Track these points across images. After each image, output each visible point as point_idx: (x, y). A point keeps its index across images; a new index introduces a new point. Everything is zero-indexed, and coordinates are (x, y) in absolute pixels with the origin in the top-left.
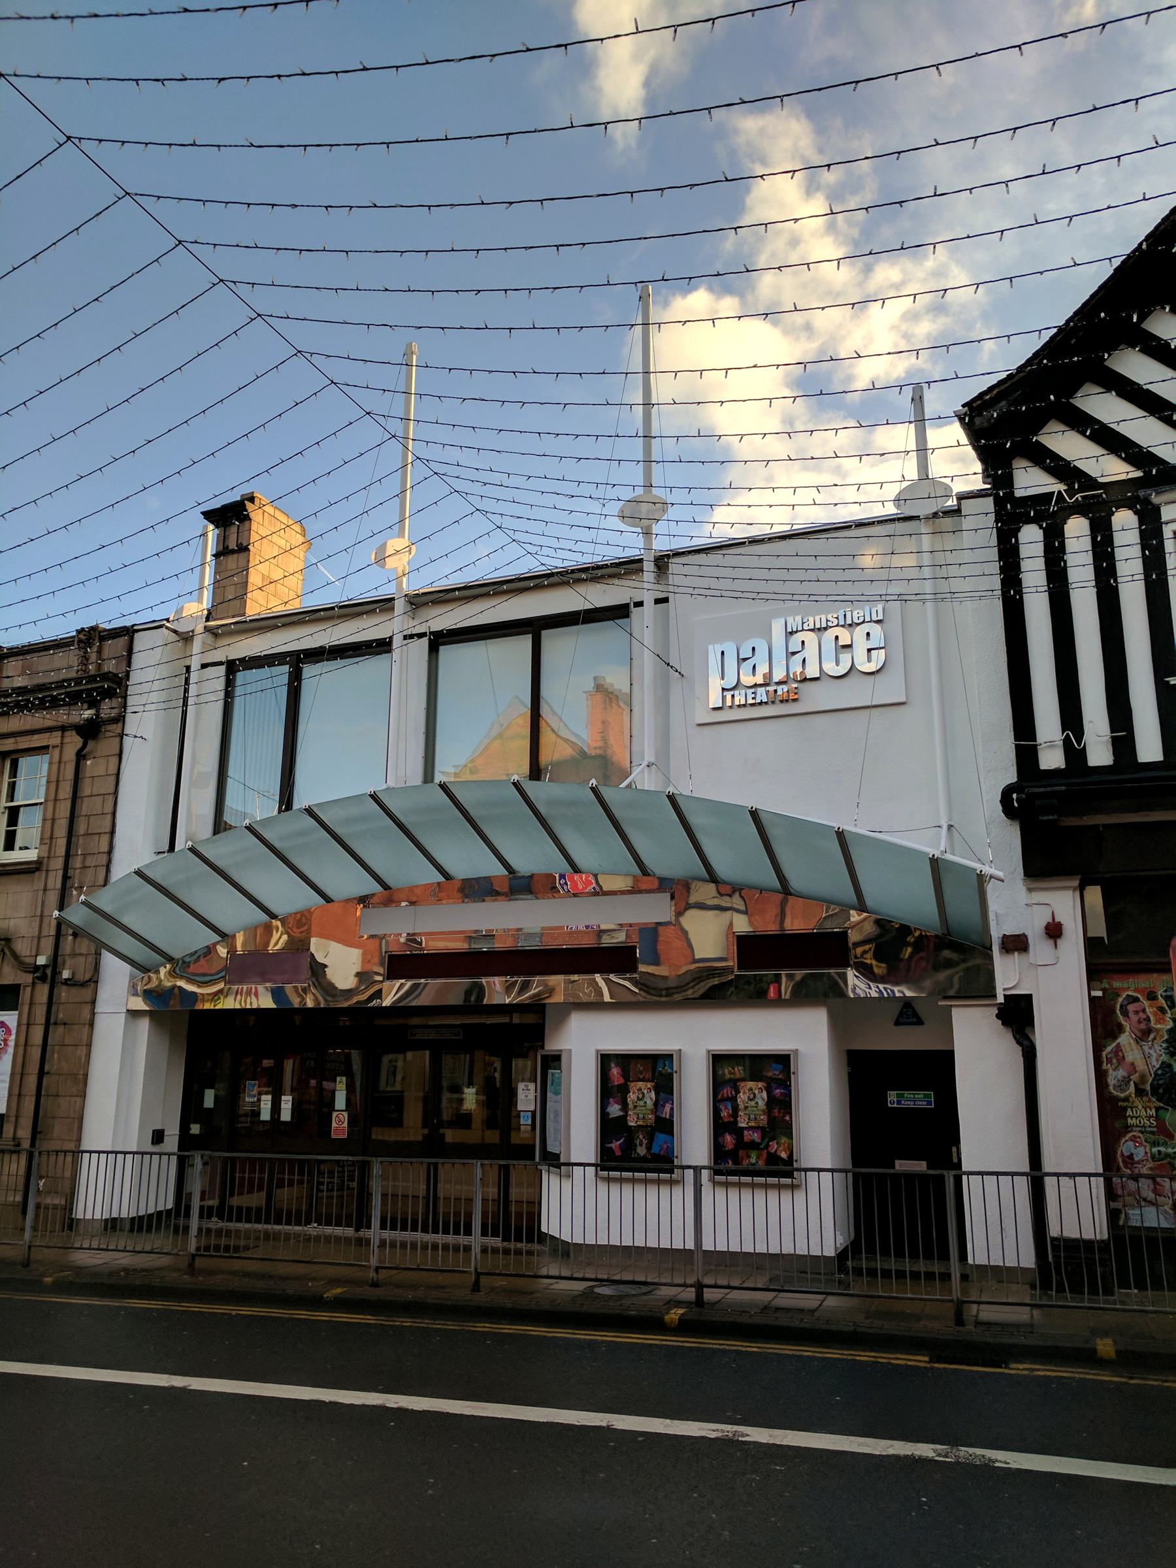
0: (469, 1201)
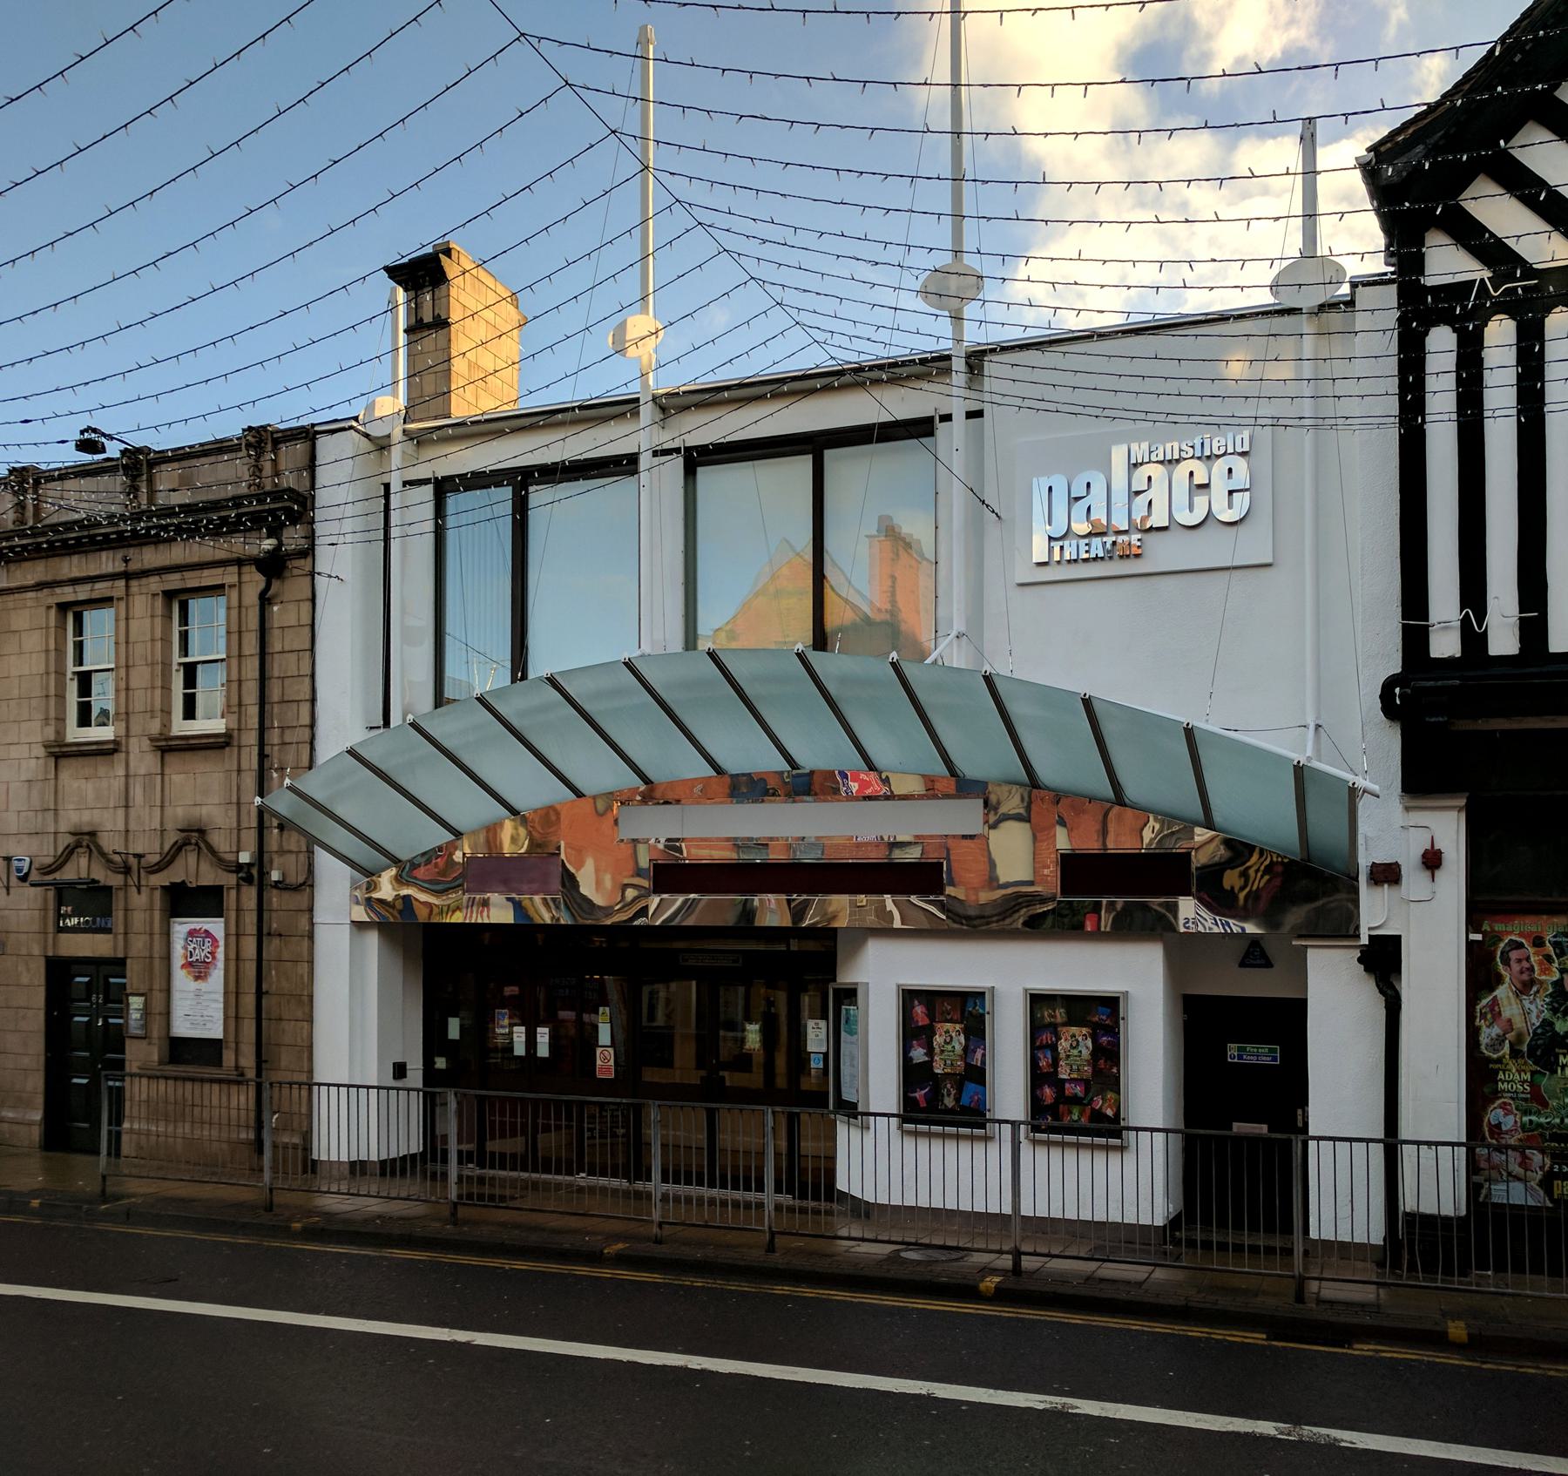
0: (761, 1154)
